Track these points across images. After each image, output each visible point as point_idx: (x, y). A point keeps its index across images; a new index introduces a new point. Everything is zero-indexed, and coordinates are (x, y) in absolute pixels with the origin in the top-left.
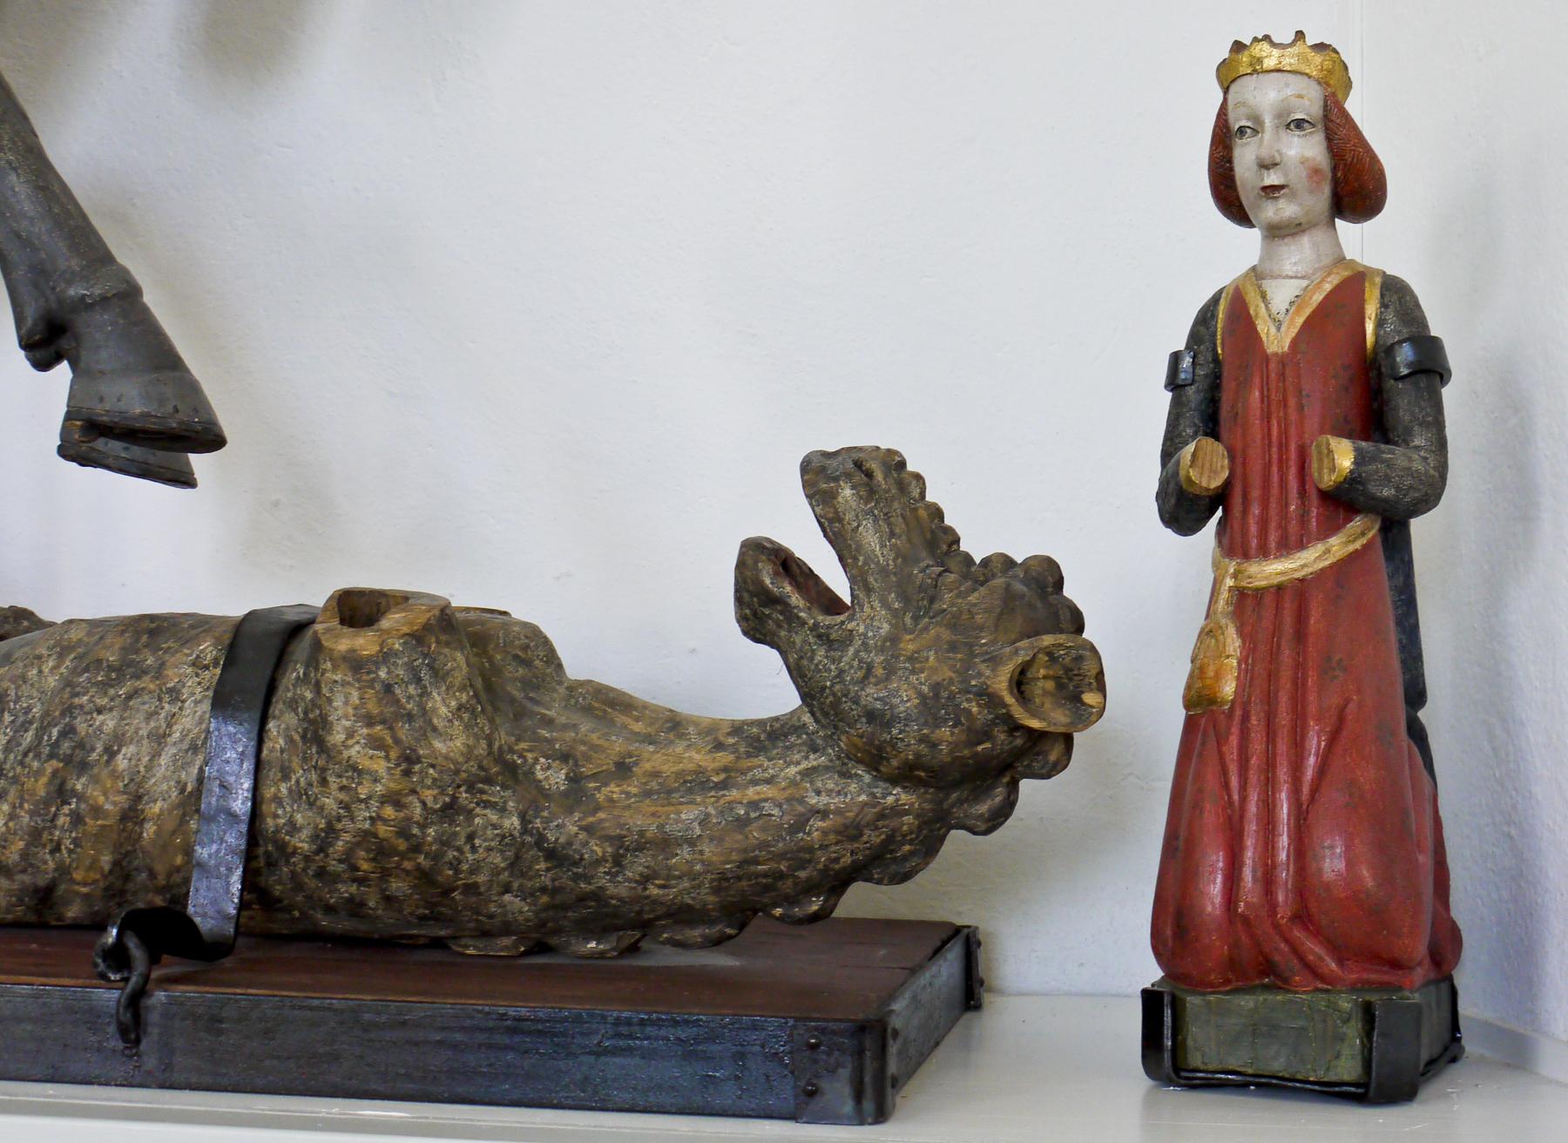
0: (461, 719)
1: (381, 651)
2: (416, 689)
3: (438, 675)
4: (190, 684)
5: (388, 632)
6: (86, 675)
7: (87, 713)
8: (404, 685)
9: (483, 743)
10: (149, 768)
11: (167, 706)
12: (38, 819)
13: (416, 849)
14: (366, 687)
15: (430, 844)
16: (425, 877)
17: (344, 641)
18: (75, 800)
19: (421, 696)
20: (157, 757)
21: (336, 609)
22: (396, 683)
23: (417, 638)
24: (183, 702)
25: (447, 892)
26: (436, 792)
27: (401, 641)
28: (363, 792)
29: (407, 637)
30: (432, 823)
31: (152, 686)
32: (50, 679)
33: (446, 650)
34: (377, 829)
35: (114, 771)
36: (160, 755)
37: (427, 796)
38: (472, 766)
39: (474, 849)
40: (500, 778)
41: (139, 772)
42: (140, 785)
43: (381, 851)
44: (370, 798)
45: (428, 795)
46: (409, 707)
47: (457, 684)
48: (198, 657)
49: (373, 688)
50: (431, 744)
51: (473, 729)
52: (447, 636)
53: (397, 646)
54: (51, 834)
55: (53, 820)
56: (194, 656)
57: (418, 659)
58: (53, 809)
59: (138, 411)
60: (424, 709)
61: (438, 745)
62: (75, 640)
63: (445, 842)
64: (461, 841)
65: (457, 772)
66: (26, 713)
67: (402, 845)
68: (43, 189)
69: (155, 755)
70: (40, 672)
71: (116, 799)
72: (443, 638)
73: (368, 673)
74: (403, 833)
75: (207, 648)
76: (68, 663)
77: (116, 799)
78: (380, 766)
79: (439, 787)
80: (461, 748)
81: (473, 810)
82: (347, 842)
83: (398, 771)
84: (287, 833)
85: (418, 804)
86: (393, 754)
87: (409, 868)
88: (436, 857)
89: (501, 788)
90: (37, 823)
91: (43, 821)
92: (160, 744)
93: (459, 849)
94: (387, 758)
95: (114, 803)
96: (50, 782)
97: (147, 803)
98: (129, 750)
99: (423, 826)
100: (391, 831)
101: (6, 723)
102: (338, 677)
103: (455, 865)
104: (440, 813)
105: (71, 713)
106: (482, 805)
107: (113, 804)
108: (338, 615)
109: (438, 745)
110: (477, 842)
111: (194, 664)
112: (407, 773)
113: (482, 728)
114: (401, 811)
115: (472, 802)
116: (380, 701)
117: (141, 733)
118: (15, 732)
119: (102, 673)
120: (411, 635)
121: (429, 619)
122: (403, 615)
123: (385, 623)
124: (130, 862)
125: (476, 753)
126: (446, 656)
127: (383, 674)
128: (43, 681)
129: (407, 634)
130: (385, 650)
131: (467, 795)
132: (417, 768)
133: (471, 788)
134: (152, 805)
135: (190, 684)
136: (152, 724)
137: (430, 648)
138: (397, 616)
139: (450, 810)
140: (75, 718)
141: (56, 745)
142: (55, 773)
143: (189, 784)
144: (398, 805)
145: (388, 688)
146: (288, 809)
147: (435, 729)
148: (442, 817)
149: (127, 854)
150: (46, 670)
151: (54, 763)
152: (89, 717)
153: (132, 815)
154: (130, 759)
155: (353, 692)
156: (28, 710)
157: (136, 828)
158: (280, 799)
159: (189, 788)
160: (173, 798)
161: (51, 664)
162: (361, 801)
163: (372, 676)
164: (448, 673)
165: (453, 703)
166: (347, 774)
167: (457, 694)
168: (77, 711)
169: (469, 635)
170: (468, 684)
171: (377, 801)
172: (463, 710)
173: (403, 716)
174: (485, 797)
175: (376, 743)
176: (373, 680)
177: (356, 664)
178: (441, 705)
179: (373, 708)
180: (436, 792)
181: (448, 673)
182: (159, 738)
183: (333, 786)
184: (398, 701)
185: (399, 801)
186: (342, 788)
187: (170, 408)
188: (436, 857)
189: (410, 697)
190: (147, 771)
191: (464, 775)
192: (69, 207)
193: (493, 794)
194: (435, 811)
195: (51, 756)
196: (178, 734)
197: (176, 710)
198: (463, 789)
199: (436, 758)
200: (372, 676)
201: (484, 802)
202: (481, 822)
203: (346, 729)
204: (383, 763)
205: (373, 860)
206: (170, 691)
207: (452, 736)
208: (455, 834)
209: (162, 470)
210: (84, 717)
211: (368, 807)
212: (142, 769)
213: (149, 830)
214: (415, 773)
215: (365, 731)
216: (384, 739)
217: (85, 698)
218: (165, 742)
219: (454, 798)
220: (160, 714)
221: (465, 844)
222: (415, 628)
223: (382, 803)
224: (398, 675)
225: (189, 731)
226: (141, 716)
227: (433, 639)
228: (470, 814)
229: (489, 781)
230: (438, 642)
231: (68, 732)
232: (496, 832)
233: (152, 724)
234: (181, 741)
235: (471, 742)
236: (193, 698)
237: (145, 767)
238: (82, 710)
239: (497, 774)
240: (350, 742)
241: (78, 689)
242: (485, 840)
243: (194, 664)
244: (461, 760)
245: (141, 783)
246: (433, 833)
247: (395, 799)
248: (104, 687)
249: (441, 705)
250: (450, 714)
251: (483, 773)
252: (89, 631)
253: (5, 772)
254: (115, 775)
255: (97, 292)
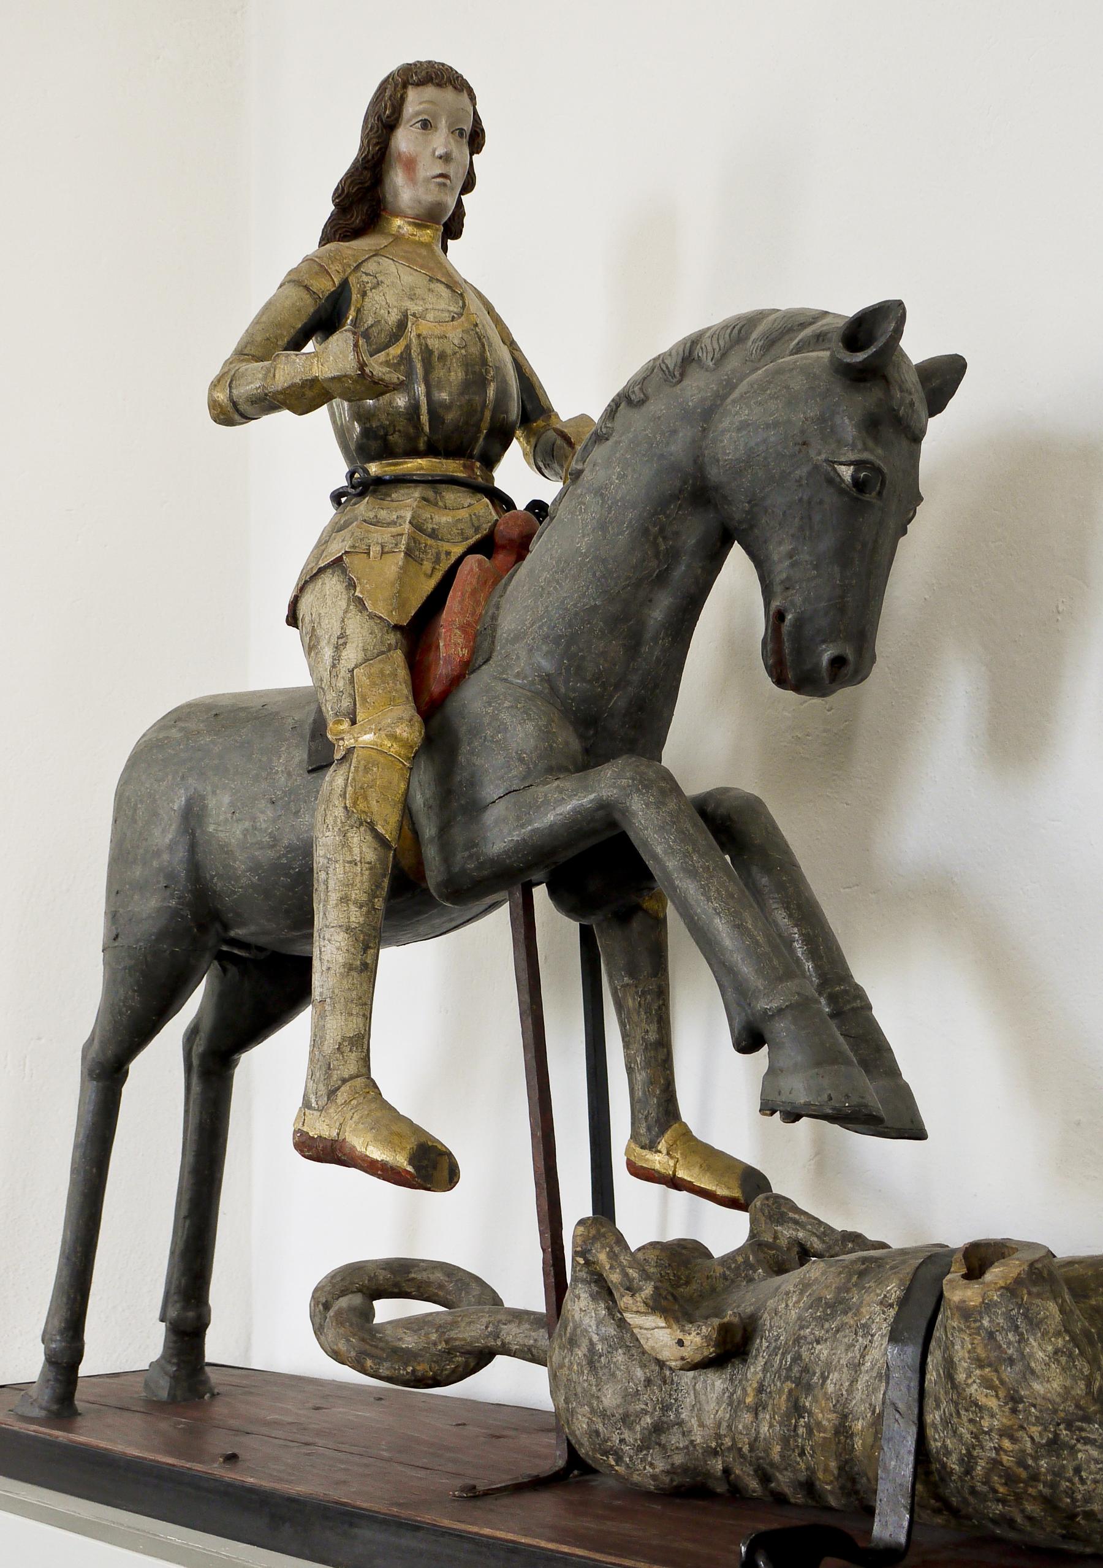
0: (1058, 1361)
1: (983, 1302)
2: (1014, 1336)
3: (1034, 1324)
4: (878, 1320)
5: (988, 1285)
6: (810, 1310)
7: (809, 1343)
8: (1004, 1332)
9: (1082, 1384)
10: (850, 1391)
11: (860, 1339)
12: (785, 1429)
13: (1035, 1477)
14: (974, 1334)
15: (1045, 1475)
16: (1049, 1503)
17: (957, 1292)
18: (806, 1415)
19: (1019, 1342)
20: (855, 1383)
21: (963, 1260)
22: (997, 1331)
23: (1011, 1290)
24: (872, 1336)
25: (1072, 1517)
26: (1040, 1428)
27: (998, 1293)
28: (986, 1424)
29: (1002, 1290)
30: (1043, 1456)
31: (852, 1322)
32: (793, 1312)
33: (1038, 1301)
34: (1001, 1459)
35: (826, 1393)
36: (857, 1381)
37: (1033, 1432)
38: (1070, 1406)
39: (1083, 1481)
40: (1098, 1416)
41: (842, 1395)
42: (844, 1405)
43: (1010, 1479)
44: (991, 1430)
45: (1035, 1430)
46: (1010, 1352)
47: (1052, 1331)
48: (885, 1296)
49: (979, 1334)
50: (1031, 1386)
51: (1071, 1371)
52: (1038, 1288)
53: (995, 1298)
54: (796, 1441)
55: (795, 1430)
56: (882, 1296)
57: (1014, 1309)
58: (793, 1421)
59: (802, 1101)
60: (1022, 1354)
61: (1036, 1386)
62: (813, 1278)
63: (1058, 1473)
64: (1070, 1473)
65: (1055, 1411)
66: (776, 1340)
67: (1024, 1475)
68: (738, 927)
69: (853, 1381)
70: (787, 1305)
71: (829, 1416)
72: (1034, 1290)
73: (975, 1321)
74: (1021, 1463)
75: (893, 1288)
76: (805, 1299)
77: (829, 1416)
78: (993, 1403)
79: (1042, 1424)
80: (1058, 1389)
81: (1075, 1445)
82: (983, 1468)
83: (1007, 1409)
84: (944, 1455)
85: (1027, 1439)
86: (1001, 1394)
87: (1034, 1494)
88: (1053, 1486)
89: (1100, 1425)
90: (784, 1432)
91: (788, 1430)
92: (856, 1372)
93: (1070, 1480)
94: (997, 1396)
95: (829, 1420)
96: (788, 1399)
97: (852, 1421)
98: (834, 1376)
99: (1036, 1459)
100: (1012, 1461)
101: (764, 1348)
102: (955, 1324)
103: (1070, 1492)
104: (1046, 1447)
105: (799, 1343)
106: (1082, 1441)
107: (827, 1419)
108: (965, 1266)
109: (1036, 1386)
110: (1083, 1474)
111: (881, 1303)
112: (1014, 1411)
113: (1081, 1370)
114: (1016, 1444)
115: (1073, 1438)
116: (985, 1346)
117: (841, 1362)
118: (769, 1356)
119: (821, 1309)
120: (1006, 1288)
121: (1019, 1274)
122: (1002, 1269)
123: (988, 1277)
124: (851, 1468)
125: (1073, 1393)
126: (1038, 1306)
127: (986, 1322)
128: (788, 1314)
129: (1002, 1287)
130: (986, 1301)
131: (1067, 1432)
132: (1021, 1406)
133: (1069, 1426)
134: (856, 1422)
135: (878, 1320)
136: (850, 1355)
137: (1023, 1299)
138: (997, 1270)
139: (1054, 1445)
140: (801, 1347)
141: (789, 1369)
142: (790, 1391)
143: (877, 1407)
144: (1013, 1439)
145: (991, 1335)
146: (942, 1435)
147: (1033, 1372)
148: (1049, 1451)
149: (846, 1462)
150: (791, 1305)
151: (789, 1383)
152: (810, 1347)
153: (843, 1430)
154: (835, 1384)
155: (966, 1338)
156: (777, 1339)
157: (848, 1441)
158: (936, 1424)
159: (877, 1411)
160: (869, 1418)
161: (794, 1299)
162: (986, 1433)
163: (978, 1324)
164: (1041, 1321)
165: (1050, 1348)
166: (971, 1409)
167: (1053, 1339)
168: (802, 1341)
169: (1069, 1282)
170: (1063, 1329)
171: (996, 1434)
172: (1060, 1354)
173: (1005, 1360)
174: (1083, 1434)
175: (987, 1384)
176: (979, 1328)
177: (966, 1313)
178: (1039, 1351)
179: (981, 1351)
180: (1040, 1428)
181: (1041, 1321)
182: (856, 1367)
183: (965, 1419)
184: (1000, 1347)
185: (1013, 1435)
186: (971, 1421)
187: (825, 1097)
188: (1053, 1486)
189: (1009, 1343)
190: (848, 1395)
191: (1062, 1415)
192: (758, 938)
193: (1092, 1432)
194: (1043, 1446)
195: (788, 1378)
196: (869, 1364)
197: (868, 1342)
198: (1062, 1427)
199: (1036, 1398)
200: (978, 1324)
201: (1083, 1438)
202: (1084, 1457)
203: (965, 1370)
204: (994, 1400)
205: (1006, 1484)
206: (864, 1326)
207: (1048, 1378)
208: (1063, 1466)
209: (886, 1130)
210: (807, 1346)
211: (991, 1438)
212: (844, 1393)
213: (858, 1443)
214: (1019, 1411)
215: (978, 1372)
216: (992, 1380)
217: (808, 1330)
218: (860, 1370)
219: (1056, 1435)
220: (855, 1346)
221: (1073, 1476)
222: (1008, 1282)
223: (1001, 1436)
224: (999, 1324)
225: (877, 1361)
226: (843, 1348)
227: (1025, 1291)
228: (1073, 1450)
229: (1087, 1419)
230: (1029, 1293)
231: (797, 1358)
232: (1099, 1466)
233: (850, 1355)
234: (872, 1369)
235: (1068, 1383)
236: (880, 1333)
237: (846, 1391)
238: (806, 1340)
239: (1096, 1413)
240: (970, 1381)
241: (804, 1323)
242: (1090, 1473)
243: (881, 1303)
244: (1058, 1400)
245: (845, 1404)
246: (1045, 1465)
247: (1006, 1433)
248: (821, 1321)
249: (1039, 1351)
250: (1047, 1358)
251: (1080, 1413)
252: (825, 1270)
253: (765, 1388)
254: (828, 1398)
255: (774, 1005)
